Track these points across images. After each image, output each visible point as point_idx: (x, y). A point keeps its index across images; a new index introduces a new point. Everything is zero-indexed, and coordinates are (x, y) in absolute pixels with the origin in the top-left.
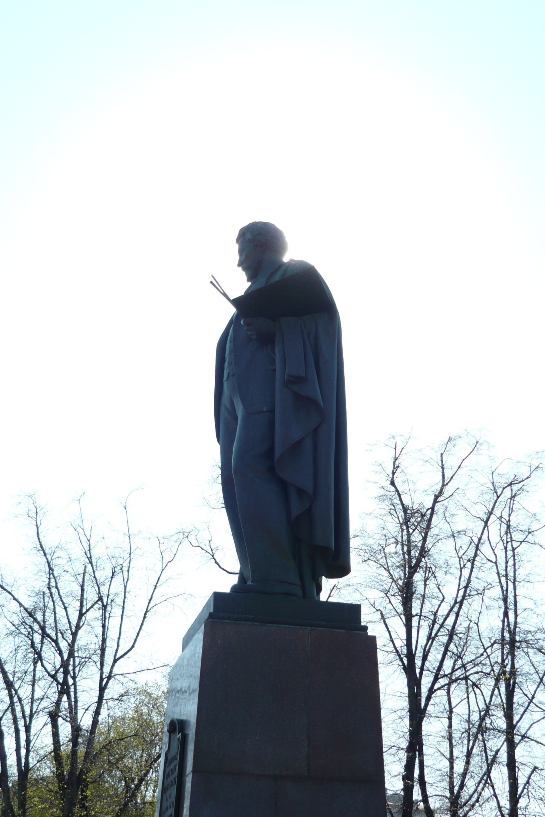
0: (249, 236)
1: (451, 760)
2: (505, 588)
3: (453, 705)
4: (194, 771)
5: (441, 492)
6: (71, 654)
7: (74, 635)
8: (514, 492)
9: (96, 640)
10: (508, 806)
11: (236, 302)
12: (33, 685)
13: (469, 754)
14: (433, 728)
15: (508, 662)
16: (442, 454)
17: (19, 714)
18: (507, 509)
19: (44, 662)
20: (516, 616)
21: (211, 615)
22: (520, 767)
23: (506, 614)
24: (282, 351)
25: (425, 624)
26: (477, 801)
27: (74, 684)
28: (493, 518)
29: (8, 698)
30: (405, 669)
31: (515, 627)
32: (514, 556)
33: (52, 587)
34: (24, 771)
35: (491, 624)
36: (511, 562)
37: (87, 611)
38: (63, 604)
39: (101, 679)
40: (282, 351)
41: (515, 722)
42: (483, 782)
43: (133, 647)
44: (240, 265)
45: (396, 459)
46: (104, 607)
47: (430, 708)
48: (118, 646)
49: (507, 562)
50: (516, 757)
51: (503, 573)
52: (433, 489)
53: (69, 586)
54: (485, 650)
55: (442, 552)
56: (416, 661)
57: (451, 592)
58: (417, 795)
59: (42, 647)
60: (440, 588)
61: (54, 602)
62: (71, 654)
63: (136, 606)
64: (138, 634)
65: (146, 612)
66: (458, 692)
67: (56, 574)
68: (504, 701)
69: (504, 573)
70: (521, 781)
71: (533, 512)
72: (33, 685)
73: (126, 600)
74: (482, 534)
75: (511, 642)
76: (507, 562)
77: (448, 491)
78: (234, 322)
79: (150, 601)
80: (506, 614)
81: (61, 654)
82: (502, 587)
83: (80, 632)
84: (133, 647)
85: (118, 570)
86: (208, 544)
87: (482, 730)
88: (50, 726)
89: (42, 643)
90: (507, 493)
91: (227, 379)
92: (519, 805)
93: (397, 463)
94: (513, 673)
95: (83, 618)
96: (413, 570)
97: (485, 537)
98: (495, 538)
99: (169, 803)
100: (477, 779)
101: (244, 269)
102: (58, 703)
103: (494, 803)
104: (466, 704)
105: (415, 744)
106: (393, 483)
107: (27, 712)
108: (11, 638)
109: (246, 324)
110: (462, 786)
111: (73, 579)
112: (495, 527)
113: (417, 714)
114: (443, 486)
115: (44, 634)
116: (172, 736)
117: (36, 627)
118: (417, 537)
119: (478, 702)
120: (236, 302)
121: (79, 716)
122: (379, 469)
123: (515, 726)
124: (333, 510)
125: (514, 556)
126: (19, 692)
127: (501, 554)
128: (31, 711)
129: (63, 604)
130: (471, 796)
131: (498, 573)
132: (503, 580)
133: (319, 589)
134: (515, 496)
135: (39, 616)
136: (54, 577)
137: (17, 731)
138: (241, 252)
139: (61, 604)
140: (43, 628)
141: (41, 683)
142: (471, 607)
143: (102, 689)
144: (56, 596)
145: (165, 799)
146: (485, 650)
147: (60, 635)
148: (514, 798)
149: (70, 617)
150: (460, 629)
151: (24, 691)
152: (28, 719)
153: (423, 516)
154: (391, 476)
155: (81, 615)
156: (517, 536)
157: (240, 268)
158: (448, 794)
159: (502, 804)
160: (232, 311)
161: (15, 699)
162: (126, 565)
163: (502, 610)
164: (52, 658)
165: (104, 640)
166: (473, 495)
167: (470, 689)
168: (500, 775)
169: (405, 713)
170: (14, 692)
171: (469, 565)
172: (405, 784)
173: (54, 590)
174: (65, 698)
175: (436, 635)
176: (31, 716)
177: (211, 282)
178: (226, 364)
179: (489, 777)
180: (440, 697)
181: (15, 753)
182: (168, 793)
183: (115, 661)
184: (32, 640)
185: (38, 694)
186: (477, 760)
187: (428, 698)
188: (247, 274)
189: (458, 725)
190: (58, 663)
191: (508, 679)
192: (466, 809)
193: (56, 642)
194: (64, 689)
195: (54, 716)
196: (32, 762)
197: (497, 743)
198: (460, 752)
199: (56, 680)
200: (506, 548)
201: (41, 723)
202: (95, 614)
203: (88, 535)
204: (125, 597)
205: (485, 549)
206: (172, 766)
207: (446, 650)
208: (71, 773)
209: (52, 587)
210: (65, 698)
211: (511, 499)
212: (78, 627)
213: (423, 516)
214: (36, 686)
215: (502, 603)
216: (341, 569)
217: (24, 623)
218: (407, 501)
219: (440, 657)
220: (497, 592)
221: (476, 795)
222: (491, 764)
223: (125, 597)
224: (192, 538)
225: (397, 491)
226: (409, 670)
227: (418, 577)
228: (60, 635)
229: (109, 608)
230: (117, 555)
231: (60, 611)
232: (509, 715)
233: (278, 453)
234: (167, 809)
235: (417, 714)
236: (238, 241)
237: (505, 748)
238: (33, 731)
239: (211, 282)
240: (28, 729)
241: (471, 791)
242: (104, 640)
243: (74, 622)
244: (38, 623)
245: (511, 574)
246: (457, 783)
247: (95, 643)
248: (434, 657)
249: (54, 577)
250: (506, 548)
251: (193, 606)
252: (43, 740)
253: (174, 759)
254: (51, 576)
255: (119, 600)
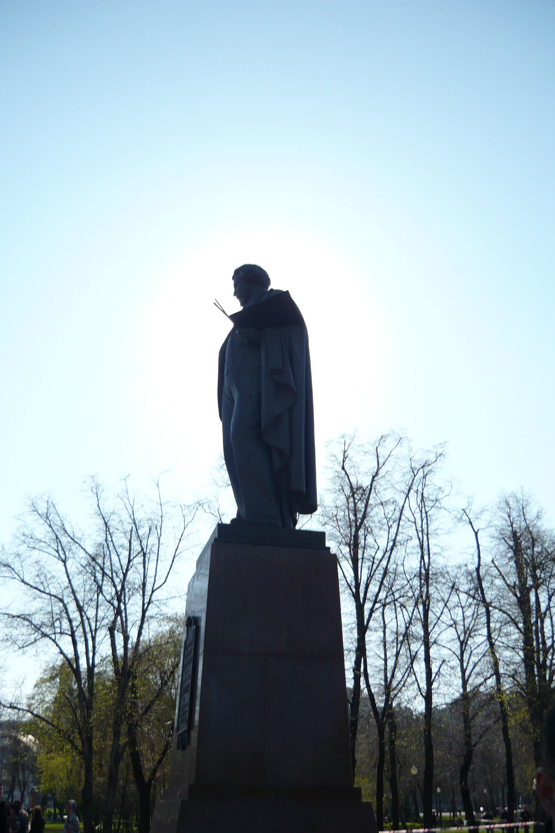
0: (241, 273)
1: (386, 660)
2: (421, 540)
3: (386, 623)
4: (205, 651)
5: (377, 474)
6: (123, 588)
7: (125, 575)
8: (425, 473)
9: (138, 576)
10: (425, 687)
11: (233, 317)
12: (97, 609)
13: (398, 654)
14: (373, 638)
15: (424, 589)
16: (377, 448)
17: (88, 629)
18: (421, 485)
19: (104, 593)
20: (429, 558)
21: (216, 540)
22: (433, 660)
23: (422, 557)
24: (266, 357)
25: (368, 564)
26: (404, 686)
27: (125, 609)
28: (412, 491)
29: (80, 618)
30: (354, 596)
31: (429, 566)
32: (427, 516)
33: (108, 542)
34: (91, 668)
35: (413, 564)
36: (425, 521)
37: (134, 558)
38: (117, 552)
39: (143, 604)
40: (266, 357)
41: (429, 631)
42: (408, 671)
43: (165, 581)
44: (235, 294)
45: (345, 452)
46: (144, 555)
47: (371, 623)
48: (155, 581)
49: (422, 521)
50: (431, 655)
51: (420, 529)
52: (371, 471)
53: (120, 539)
54: (409, 582)
55: (377, 514)
56: (360, 594)
57: (383, 543)
58: (363, 685)
59: (102, 582)
60: (376, 541)
61: (110, 551)
62: (123, 588)
63: (167, 552)
64: (168, 573)
65: (174, 557)
66: (389, 614)
67: (111, 531)
68: (422, 617)
69: (421, 529)
70: (434, 670)
71: (439, 486)
72: (97, 609)
73: (160, 549)
74: (405, 502)
75: (425, 576)
76: (422, 521)
77: (382, 472)
78: (232, 335)
79: (176, 550)
80: (422, 557)
81: (115, 586)
82: (419, 539)
83: (129, 573)
84: (165, 581)
85: (153, 528)
86: (217, 510)
87: (406, 635)
88: (109, 636)
89: (103, 580)
90: (421, 474)
91: (227, 374)
92: (433, 687)
93: (346, 454)
94: (428, 597)
95: (131, 563)
96: (358, 529)
97: (407, 505)
98: (414, 506)
99: (188, 675)
100: (402, 671)
101: (238, 297)
102: (114, 622)
103: (416, 686)
104: (395, 620)
105: (361, 651)
106: (343, 468)
107: (93, 628)
108: (80, 576)
109: (239, 333)
110: (393, 676)
111: (122, 535)
112: (413, 499)
113: (362, 628)
114: (378, 469)
115: (104, 574)
116: (189, 628)
117: (98, 568)
118: (361, 506)
119: (403, 617)
120: (233, 317)
121: (129, 629)
122: (334, 458)
123: (430, 633)
124: (304, 441)
125: (427, 516)
126: (87, 613)
127: (418, 516)
128: (96, 626)
129: (117, 552)
130: (399, 683)
131: (417, 530)
132: (420, 534)
133: (295, 522)
134: (426, 475)
135: (100, 561)
136: (110, 534)
137: (86, 640)
138: (235, 285)
139: (114, 551)
140: (102, 569)
141: (102, 608)
142: (398, 553)
143: (144, 611)
144: (111, 548)
145: (184, 675)
146: (409, 582)
147: (114, 574)
148: (429, 683)
149: (122, 563)
150: (391, 567)
151: (91, 613)
152: (94, 633)
153: (364, 491)
154: (342, 463)
155: (129, 561)
156: (429, 504)
157: (235, 297)
158: (383, 683)
159: (421, 686)
160: (230, 325)
161: (85, 618)
162: (159, 525)
163: (420, 555)
164: (109, 590)
165: (145, 577)
166: (397, 476)
167: (399, 609)
168: (420, 667)
169: (355, 625)
170: (84, 614)
171: (395, 525)
172: (355, 674)
173: (111, 544)
174: (119, 618)
175: (373, 574)
176: (96, 630)
177: (215, 304)
178: (226, 364)
179: (412, 667)
180: (377, 614)
181: (85, 655)
182: (187, 668)
183: (153, 591)
184: (95, 577)
185: (101, 614)
186: (403, 660)
187: (370, 615)
188: (240, 301)
189: (390, 638)
190: (114, 593)
191: (424, 601)
192: (395, 692)
193: (112, 579)
194: (118, 612)
195: (111, 630)
196: (97, 661)
197: (417, 647)
198: (391, 652)
199: (112, 604)
200: (421, 512)
201: (103, 635)
202: (140, 559)
203: (132, 503)
204: (159, 547)
205: (407, 513)
206: (189, 650)
207: (382, 583)
208: (123, 667)
209: (108, 542)
210: (119, 618)
211: (424, 477)
212: (127, 570)
213: (364, 491)
214: (99, 609)
215: (419, 550)
216: (310, 507)
217: (89, 565)
218: (353, 480)
219: (376, 590)
220: (416, 542)
221: (402, 683)
222: (413, 658)
223: (159, 547)
224: (205, 507)
225: (346, 473)
226: (356, 596)
227: (361, 532)
228: (114, 574)
229: (147, 556)
230: (153, 518)
231: (115, 558)
232: (425, 626)
233: (263, 425)
234: (186, 680)
235: (362, 628)
236: (233, 278)
237: (423, 648)
238: (98, 639)
239: (215, 304)
240: (94, 639)
241: (399, 679)
242: (145, 577)
243: (125, 567)
244: (99, 565)
245: (425, 530)
246: (389, 675)
247: (138, 581)
248: (373, 588)
249: (110, 534)
250: (421, 512)
251: (203, 533)
252: (104, 649)
253: (190, 644)
254: (108, 533)
255: (155, 549)
